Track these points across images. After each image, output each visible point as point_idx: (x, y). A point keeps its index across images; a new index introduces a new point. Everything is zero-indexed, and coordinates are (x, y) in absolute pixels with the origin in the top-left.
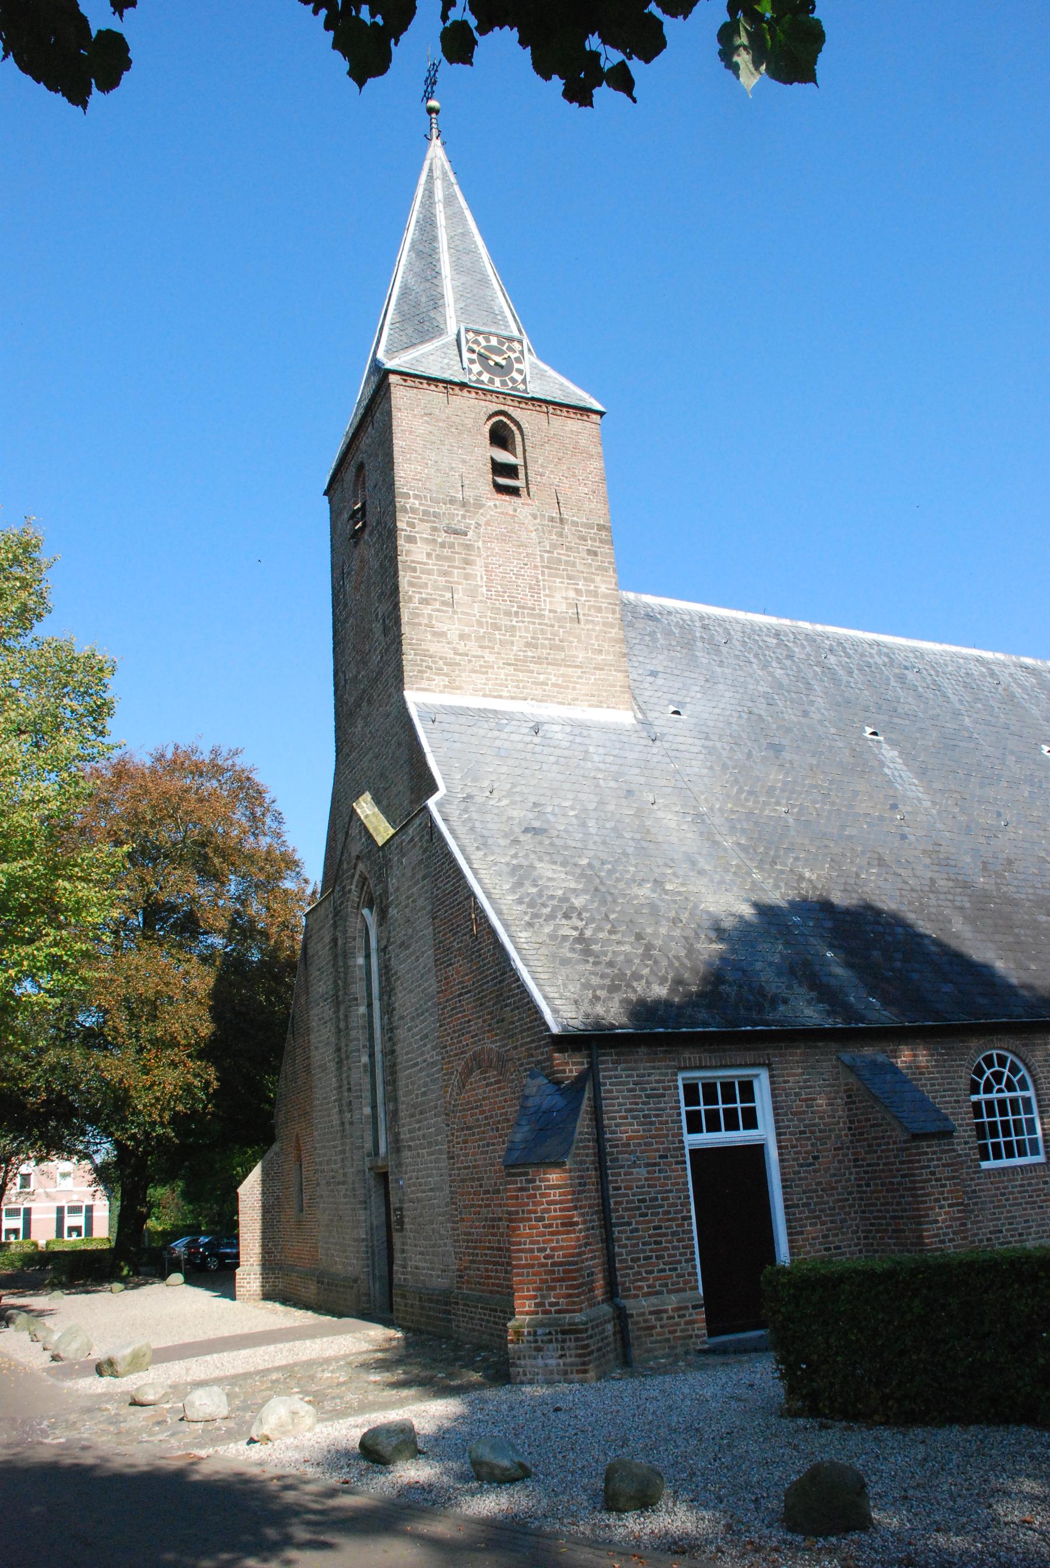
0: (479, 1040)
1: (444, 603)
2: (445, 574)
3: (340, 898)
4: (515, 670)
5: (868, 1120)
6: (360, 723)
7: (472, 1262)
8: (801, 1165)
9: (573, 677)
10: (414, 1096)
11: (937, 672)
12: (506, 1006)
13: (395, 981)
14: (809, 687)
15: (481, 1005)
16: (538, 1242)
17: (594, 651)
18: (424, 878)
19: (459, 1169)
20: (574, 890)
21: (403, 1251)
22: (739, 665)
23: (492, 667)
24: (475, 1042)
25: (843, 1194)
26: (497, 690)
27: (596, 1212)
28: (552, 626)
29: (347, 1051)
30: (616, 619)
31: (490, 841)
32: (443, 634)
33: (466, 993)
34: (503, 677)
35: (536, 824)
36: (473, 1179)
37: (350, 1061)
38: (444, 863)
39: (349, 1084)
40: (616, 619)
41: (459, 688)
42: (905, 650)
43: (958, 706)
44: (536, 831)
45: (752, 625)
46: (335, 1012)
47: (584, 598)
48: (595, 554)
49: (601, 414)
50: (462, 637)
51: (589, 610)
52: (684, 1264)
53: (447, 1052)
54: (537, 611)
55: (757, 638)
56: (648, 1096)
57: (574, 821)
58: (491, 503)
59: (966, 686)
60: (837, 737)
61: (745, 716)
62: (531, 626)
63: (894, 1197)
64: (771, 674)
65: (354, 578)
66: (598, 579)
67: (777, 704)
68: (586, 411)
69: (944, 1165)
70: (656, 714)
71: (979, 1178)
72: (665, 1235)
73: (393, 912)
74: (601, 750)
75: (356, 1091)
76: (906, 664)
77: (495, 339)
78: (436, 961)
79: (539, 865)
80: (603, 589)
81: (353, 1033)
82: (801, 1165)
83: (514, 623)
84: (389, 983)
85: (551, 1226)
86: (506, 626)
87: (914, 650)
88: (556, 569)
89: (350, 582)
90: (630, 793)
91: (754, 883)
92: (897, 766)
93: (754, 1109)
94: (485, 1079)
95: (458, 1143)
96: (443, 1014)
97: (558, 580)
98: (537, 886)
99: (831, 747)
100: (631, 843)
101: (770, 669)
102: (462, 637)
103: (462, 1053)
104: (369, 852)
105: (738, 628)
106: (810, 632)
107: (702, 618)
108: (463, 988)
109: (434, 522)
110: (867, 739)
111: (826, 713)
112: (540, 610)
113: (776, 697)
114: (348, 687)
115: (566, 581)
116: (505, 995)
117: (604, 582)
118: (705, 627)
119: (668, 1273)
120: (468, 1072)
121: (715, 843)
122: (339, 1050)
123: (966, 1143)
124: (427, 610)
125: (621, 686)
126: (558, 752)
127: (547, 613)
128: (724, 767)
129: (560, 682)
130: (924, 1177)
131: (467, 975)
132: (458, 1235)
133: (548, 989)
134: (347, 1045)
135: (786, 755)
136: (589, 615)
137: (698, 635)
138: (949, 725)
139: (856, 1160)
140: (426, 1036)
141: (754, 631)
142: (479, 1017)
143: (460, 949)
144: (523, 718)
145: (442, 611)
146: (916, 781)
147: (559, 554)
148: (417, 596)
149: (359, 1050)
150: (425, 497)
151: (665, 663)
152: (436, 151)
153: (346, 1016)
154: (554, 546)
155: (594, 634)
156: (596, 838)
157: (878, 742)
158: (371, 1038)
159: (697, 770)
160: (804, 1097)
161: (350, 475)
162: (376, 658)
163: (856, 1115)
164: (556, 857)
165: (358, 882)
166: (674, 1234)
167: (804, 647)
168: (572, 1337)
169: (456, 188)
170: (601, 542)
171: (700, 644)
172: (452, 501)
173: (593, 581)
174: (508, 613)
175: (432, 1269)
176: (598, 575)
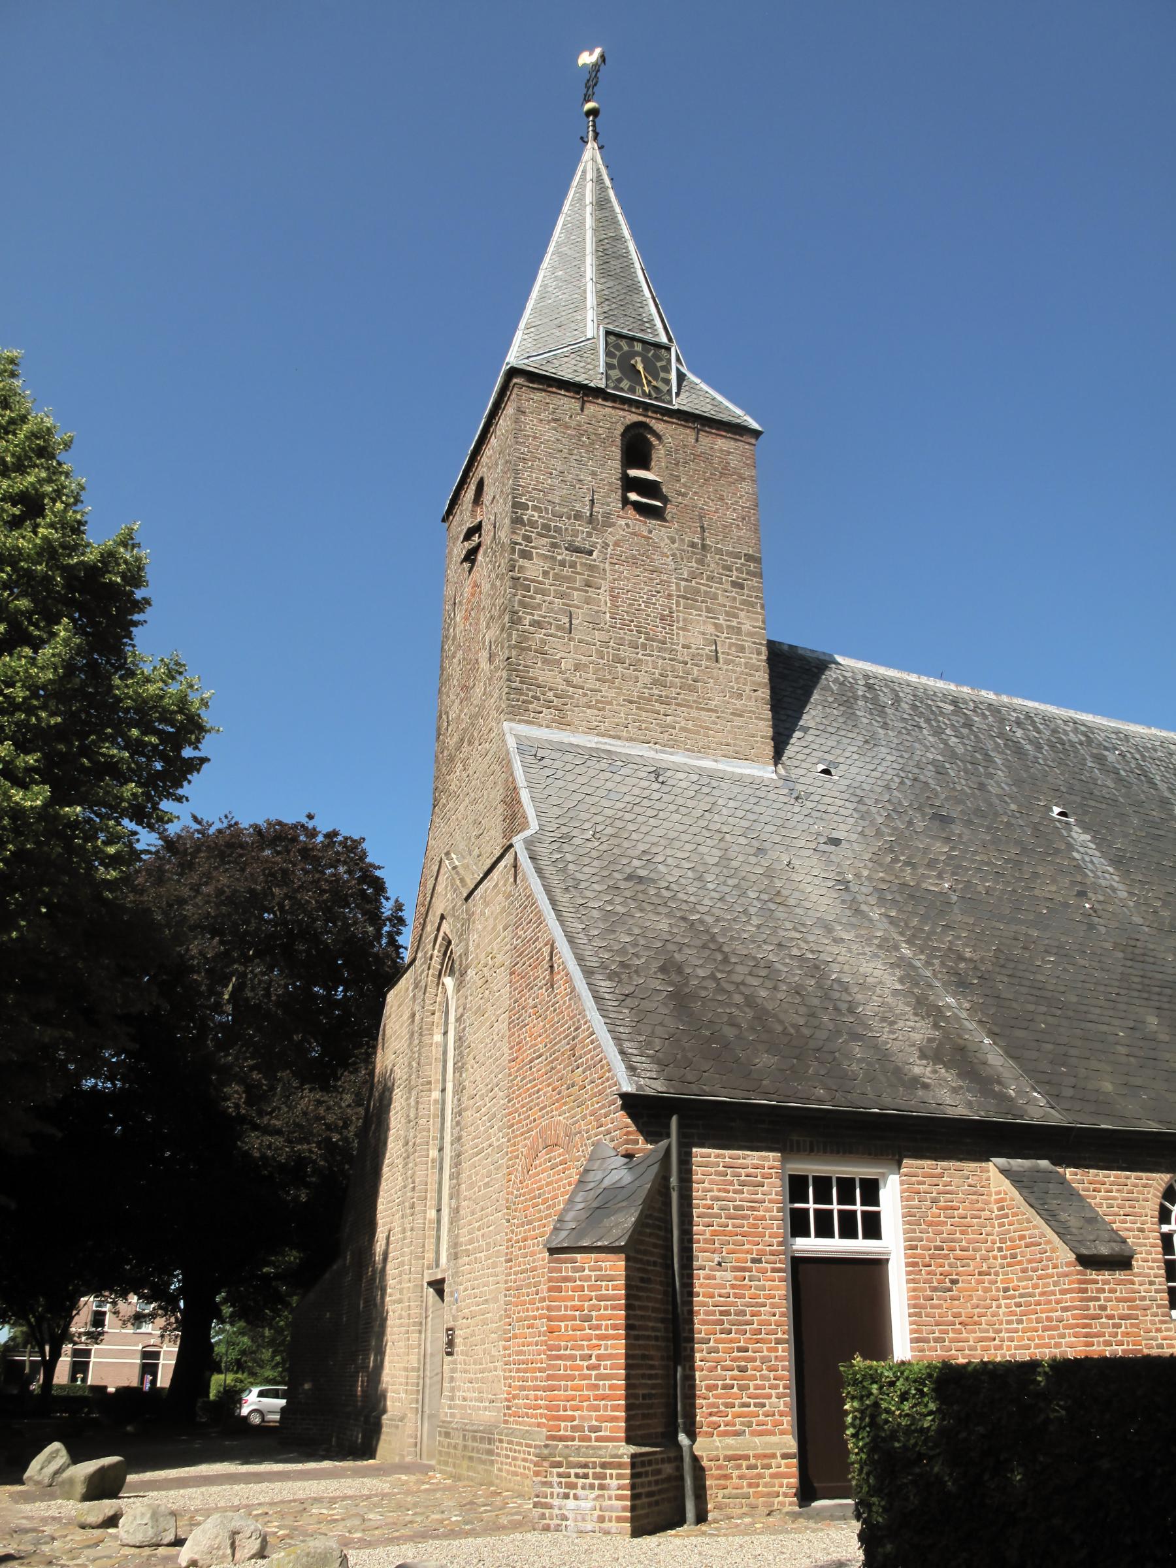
1: (559, 628)
2: (561, 595)
4: (638, 708)
5: (1022, 1238)
7: (522, 1388)
8: (935, 1289)
9: (704, 721)
11: (1143, 756)
14: (988, 758)
16: (581, 1348)
19: (516, 1273)
21: (452, 1379)
25: (987, 1331)
27: (663, 1321)
36: (529, 1286)
39: (413, 1182)
43: (1167, 794)
47: (725, 635)
48: (742, 587)
49: (756, 434)
51: (729, 649)
52: (774, 1400)
53: (513, 1132)
55: (930, 702)
56: (743, 1184)
58: (623, 522)
60: (1018, 815)
61: (909, 783)
62: (660, 661)
63: (1051, 1337)
65: (464, 607)
66: (742, 614)
67: (947, 774)
68: (737, 430)
69: (1118, 1300)
70: (803, 772)
71: (1168, 1330)
72: (754, 1360)
77: (640, 345)
78: (510, 1024)
80: (747, 627)
82: (935, 1289)
85: (598, 1327)
87: (1117, 732)
88: (692, 600)
92: (1090, 851)
93: (877, 1214)
99: (1009, 825)
101: (944, 736)
102: (577, 667)
106: (995, 703)
107: (866, 676)
111: (1006, 788)
113: (948, 766)
115: (704, 614)
118: (870, 687)
119: (752, 1408)
121: (857, 911)
123: (1151, 1283)
127: (679, 648)
129: (689, 727)
130: (1091, 1312)
132: (509, 1356)
133: (627, 1044)
136: (728, 654)
137: (860, 693)
138: (1154, 813)
139: (1006, 1290)
144: (641, 763)
146: (1111, 869)
147: (697, 583)
151: (818, 720)
154: (693, 575)
157: (1068, 823)
160: (942, 1204)
161: (469, 494)
163: (1009, 1232)
164: (661, 909)
166: (764, 1360)
168: (614, 1472)
169: (611, 193)
170: (747, 574)
172: (578, 516)
175: (480, 1400)
176: (742, 610)
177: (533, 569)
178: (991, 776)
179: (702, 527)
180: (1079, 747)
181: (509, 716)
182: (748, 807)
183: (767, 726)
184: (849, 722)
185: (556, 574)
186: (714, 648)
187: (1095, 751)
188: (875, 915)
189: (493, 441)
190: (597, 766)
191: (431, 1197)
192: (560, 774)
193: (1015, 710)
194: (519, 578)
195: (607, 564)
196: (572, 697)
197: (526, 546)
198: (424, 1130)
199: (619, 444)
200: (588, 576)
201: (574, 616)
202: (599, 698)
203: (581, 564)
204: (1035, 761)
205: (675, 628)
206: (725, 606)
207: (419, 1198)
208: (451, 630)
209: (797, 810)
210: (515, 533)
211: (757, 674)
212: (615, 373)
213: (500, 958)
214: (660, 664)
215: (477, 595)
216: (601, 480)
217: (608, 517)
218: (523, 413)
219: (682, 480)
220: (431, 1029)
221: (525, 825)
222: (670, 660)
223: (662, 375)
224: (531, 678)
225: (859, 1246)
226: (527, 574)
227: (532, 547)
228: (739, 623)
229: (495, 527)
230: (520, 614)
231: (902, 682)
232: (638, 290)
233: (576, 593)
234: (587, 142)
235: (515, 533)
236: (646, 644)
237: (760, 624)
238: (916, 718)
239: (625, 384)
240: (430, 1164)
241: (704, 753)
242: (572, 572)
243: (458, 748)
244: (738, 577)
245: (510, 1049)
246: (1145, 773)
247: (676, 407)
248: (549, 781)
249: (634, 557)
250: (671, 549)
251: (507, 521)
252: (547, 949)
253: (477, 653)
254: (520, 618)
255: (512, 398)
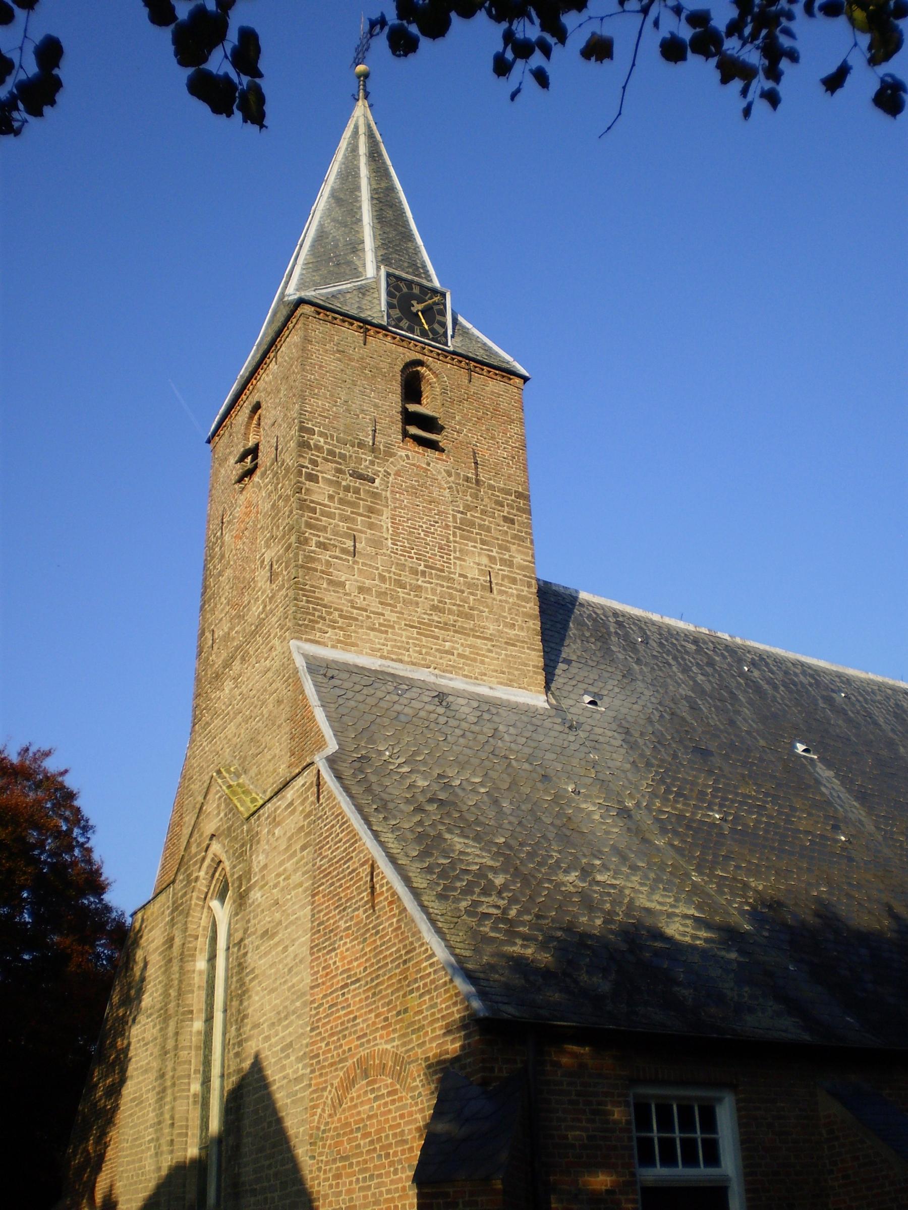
0: (368, 1041)
1: (344, 551)
2: (346, 519)
3: (182, 888)
6: (228, 685)
9: (481, 649)
10: (265, 1125)
12: (412, 992)
13: (252, 980)
14: (733, 695)
15: (374, 994)
17: (506, 625)
18: (303, 848)
20: (491, 868)
22: (658, 666)
23: (393, 627)
24: (362, 1045)
26: (394, 653)
28: (462, 592)
29: (173, 1077)
30: (531, 593)
31: (391, 805)
32: (342, 585)
33: (353, 983)
34: (404, 639)
35: (442, 796)
37: (176, 1089)
38: (333, 826)
39: (172, 1118)
40: (531, 593)
41: (353, 645)
42: (831, 674)
43: (891, 734)
44: (441, 802)
45: (669, 629)
46: (161, 1029)
47: (498, 567)
48: (512, 522)
49: (525, 379)
50: (361, 590)
51: (503, 580)
54: (447, 573)
55: (675, 642)
57: (486, 798)
58: (403, 453)
59: (896, 715)
62: (439, 589)
64: (693, 679)
66: (513, 548)
68: (508, 373)
70: (571, 702)
73: (256, 895)
74: (512, 730)
75: (181, 1127)
76: (833, 687)
78: (312, 948)
79: (447, 836)
81: (183, 1054)
83: (420, 583)
84: (243, 984)
86: (411, 585)
88: (468, 531)
89: (231, 531)
90: (545, 777)
91: (694, 885)
94: (373, 1091)
95: (326, 1180)
96: (318, 1013)
97: (471, 544)
98: (449, 857)
100: (551, 828)
103: (341, 1061)
104: (229, 828)
105: (654, 629)
106: (731, 645)
107: (615, 614)
108: (349, 977)
109: (340, 464)
110: (799, 756)
111: (754, 725)
112: (450, 573)
114: (215, 647)
115: (479, 545)
116: (410, 979)
117: (519, 551)
118: (620, 624)
120: (349, 1083)
121: (644, 840)
122: (162, 1076)
124: (325, 556)
125: (534, 666)
126: (464, 725)
127: (456, 577)
128: (648, 764)
129: (467, 653)
131: (356, 959)
134: (174, 1069)
135: (717, 761)
136: (502, 585)
137: (612, 630)
140: (290, 1045)
141: (672, 635)
142: (371, 1011)
143: (348, 928)
144: (424, 686)
145: (341, 559)
147: (472, 515)
148: (315, 538)
149: (189, 1076)
150: (332, 436)
151: (579, 653)
152: (361, 112)
153: (177, 1034)
154: (468, 508)
155: (507, 606)
156: (512, 819)
157: (812, 759)
158: (207, 1063)
159: (619, 764)
162: (256, 610)
165: (209, 866)
167: (724, 657)
170: (518, 510)
171: (614, 639)
172: (361, 445)
173: (508, 550)
174: (414, 572)
176: (514, 544)
177: (320, 493)
178: (738, 713)
179: (476, 463)
180: (810, 688)
181: (297, 634)
182: (528, 734)
183: (539, 656)
184: (607, 656)
185: (340, 499)
186: (488, 579)
187: (824, 693)
188: (660, 842)
189: (273, 367)
190: (383, 688)
191: (193, 1135)
192: (350, 694)
193: (749, 652)
194: (305, 500)
195: (388, 493)
196: (357, 620)
197: (313, 470)
198: (185, 1062)
199: (399, 378)
200: (372, 502)
201: (357, 540)
202: (382, 621)
203: (365, 490)
204: (774, 699)
205: (452, 557)
206: (498, 539)
207: (180, 1135)
208: (217, 549)
209: (572, 738)
210: (303, 457)
211: (528, 605)
212: (396, 313)
213: (297, 878)
214: (438, 591)
215: (253, 515)
216: (383, 411)
217: (389, 448)
218: (310, 342)
219: (457, 418)
220: (193, 956)
221: (321, 744)
222: (448, 587)
223: (439, 318)
224: (317, 598)
225: (702, 1172)
226: (315, 497)
227: (318, 471)
228: (510, 556)
229: (277, 450)
230: (307, 535)
231: (647, 621)
232: (409, 237)
233: (359, 518)
234: (358, 100)
235: (303, 457)
236: (425, 572)
237: (529, 559)
238: (664, 655)
239: (405, 323)
240: (191, 1100)
241: (482, 679)
242: (356, 498)
243: (227, 664)
244: (508, 513)
245: (312, 975)
246: (870, 715)
247: (451, 349)
248: (341, 701)
249: (413, 487)
250: (448, 482)
251: (292, 444)
252: (367, 868)
253: (254, 571)
254: (306, 539)
255: (297, 326)
